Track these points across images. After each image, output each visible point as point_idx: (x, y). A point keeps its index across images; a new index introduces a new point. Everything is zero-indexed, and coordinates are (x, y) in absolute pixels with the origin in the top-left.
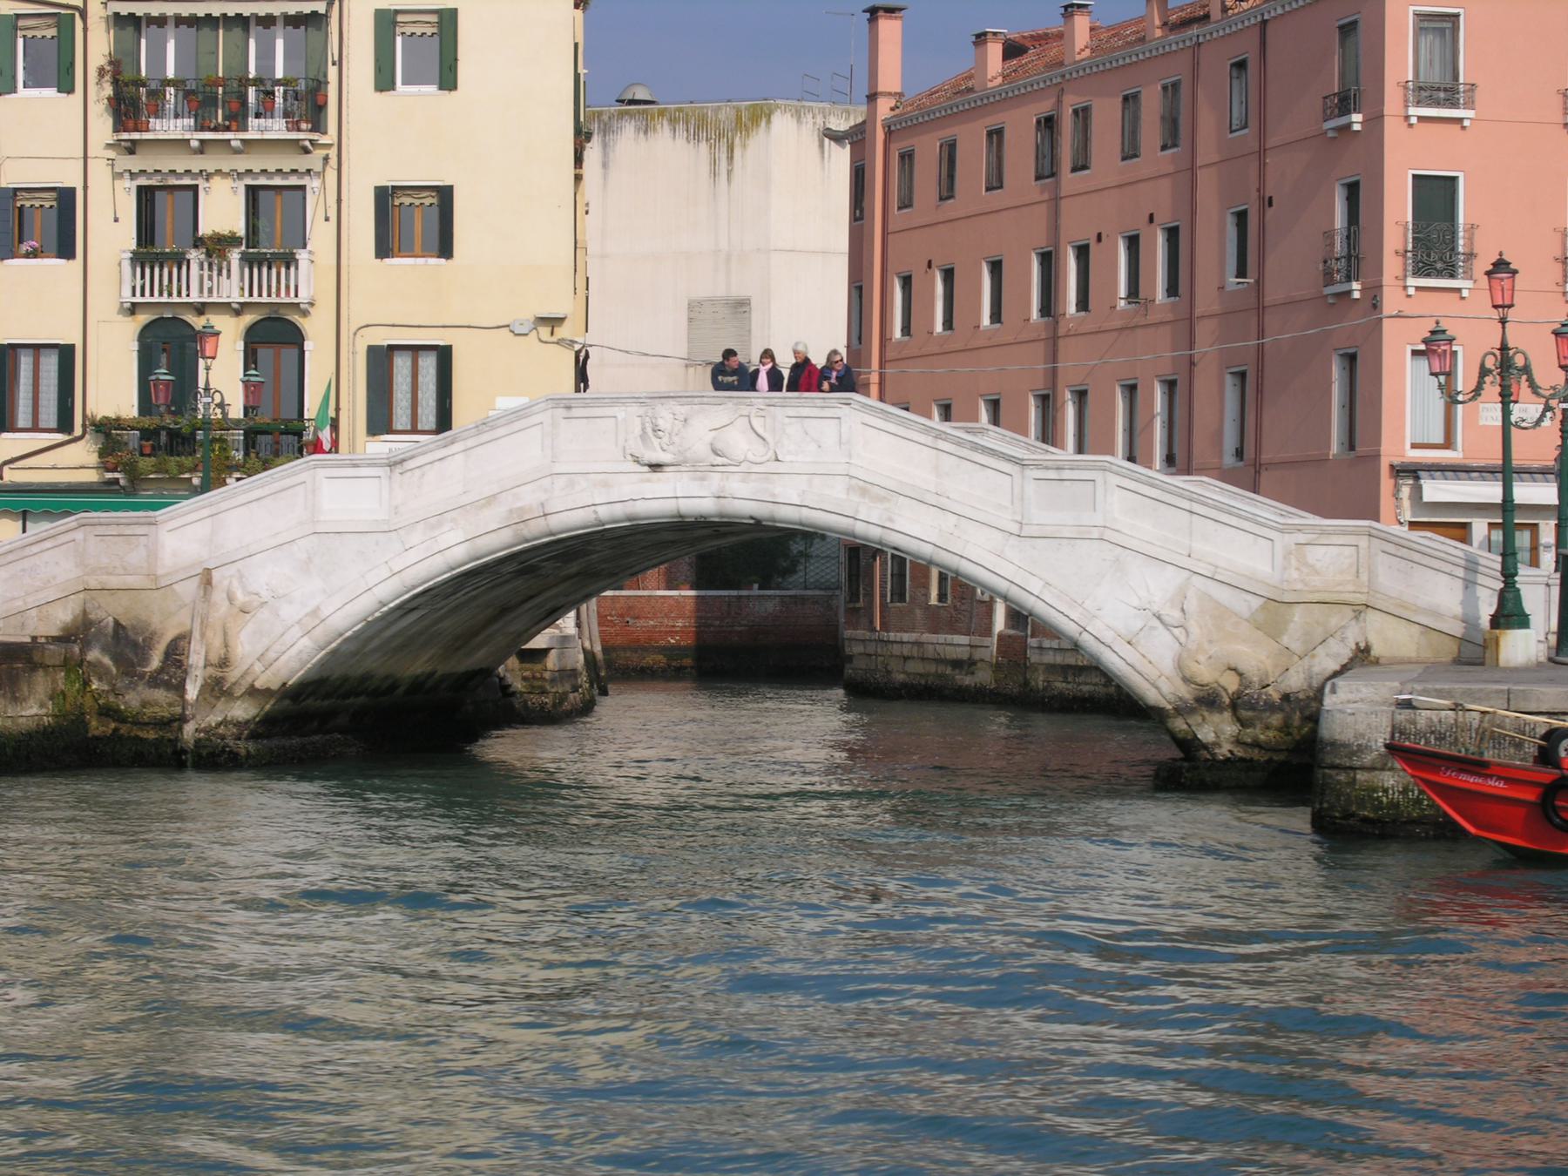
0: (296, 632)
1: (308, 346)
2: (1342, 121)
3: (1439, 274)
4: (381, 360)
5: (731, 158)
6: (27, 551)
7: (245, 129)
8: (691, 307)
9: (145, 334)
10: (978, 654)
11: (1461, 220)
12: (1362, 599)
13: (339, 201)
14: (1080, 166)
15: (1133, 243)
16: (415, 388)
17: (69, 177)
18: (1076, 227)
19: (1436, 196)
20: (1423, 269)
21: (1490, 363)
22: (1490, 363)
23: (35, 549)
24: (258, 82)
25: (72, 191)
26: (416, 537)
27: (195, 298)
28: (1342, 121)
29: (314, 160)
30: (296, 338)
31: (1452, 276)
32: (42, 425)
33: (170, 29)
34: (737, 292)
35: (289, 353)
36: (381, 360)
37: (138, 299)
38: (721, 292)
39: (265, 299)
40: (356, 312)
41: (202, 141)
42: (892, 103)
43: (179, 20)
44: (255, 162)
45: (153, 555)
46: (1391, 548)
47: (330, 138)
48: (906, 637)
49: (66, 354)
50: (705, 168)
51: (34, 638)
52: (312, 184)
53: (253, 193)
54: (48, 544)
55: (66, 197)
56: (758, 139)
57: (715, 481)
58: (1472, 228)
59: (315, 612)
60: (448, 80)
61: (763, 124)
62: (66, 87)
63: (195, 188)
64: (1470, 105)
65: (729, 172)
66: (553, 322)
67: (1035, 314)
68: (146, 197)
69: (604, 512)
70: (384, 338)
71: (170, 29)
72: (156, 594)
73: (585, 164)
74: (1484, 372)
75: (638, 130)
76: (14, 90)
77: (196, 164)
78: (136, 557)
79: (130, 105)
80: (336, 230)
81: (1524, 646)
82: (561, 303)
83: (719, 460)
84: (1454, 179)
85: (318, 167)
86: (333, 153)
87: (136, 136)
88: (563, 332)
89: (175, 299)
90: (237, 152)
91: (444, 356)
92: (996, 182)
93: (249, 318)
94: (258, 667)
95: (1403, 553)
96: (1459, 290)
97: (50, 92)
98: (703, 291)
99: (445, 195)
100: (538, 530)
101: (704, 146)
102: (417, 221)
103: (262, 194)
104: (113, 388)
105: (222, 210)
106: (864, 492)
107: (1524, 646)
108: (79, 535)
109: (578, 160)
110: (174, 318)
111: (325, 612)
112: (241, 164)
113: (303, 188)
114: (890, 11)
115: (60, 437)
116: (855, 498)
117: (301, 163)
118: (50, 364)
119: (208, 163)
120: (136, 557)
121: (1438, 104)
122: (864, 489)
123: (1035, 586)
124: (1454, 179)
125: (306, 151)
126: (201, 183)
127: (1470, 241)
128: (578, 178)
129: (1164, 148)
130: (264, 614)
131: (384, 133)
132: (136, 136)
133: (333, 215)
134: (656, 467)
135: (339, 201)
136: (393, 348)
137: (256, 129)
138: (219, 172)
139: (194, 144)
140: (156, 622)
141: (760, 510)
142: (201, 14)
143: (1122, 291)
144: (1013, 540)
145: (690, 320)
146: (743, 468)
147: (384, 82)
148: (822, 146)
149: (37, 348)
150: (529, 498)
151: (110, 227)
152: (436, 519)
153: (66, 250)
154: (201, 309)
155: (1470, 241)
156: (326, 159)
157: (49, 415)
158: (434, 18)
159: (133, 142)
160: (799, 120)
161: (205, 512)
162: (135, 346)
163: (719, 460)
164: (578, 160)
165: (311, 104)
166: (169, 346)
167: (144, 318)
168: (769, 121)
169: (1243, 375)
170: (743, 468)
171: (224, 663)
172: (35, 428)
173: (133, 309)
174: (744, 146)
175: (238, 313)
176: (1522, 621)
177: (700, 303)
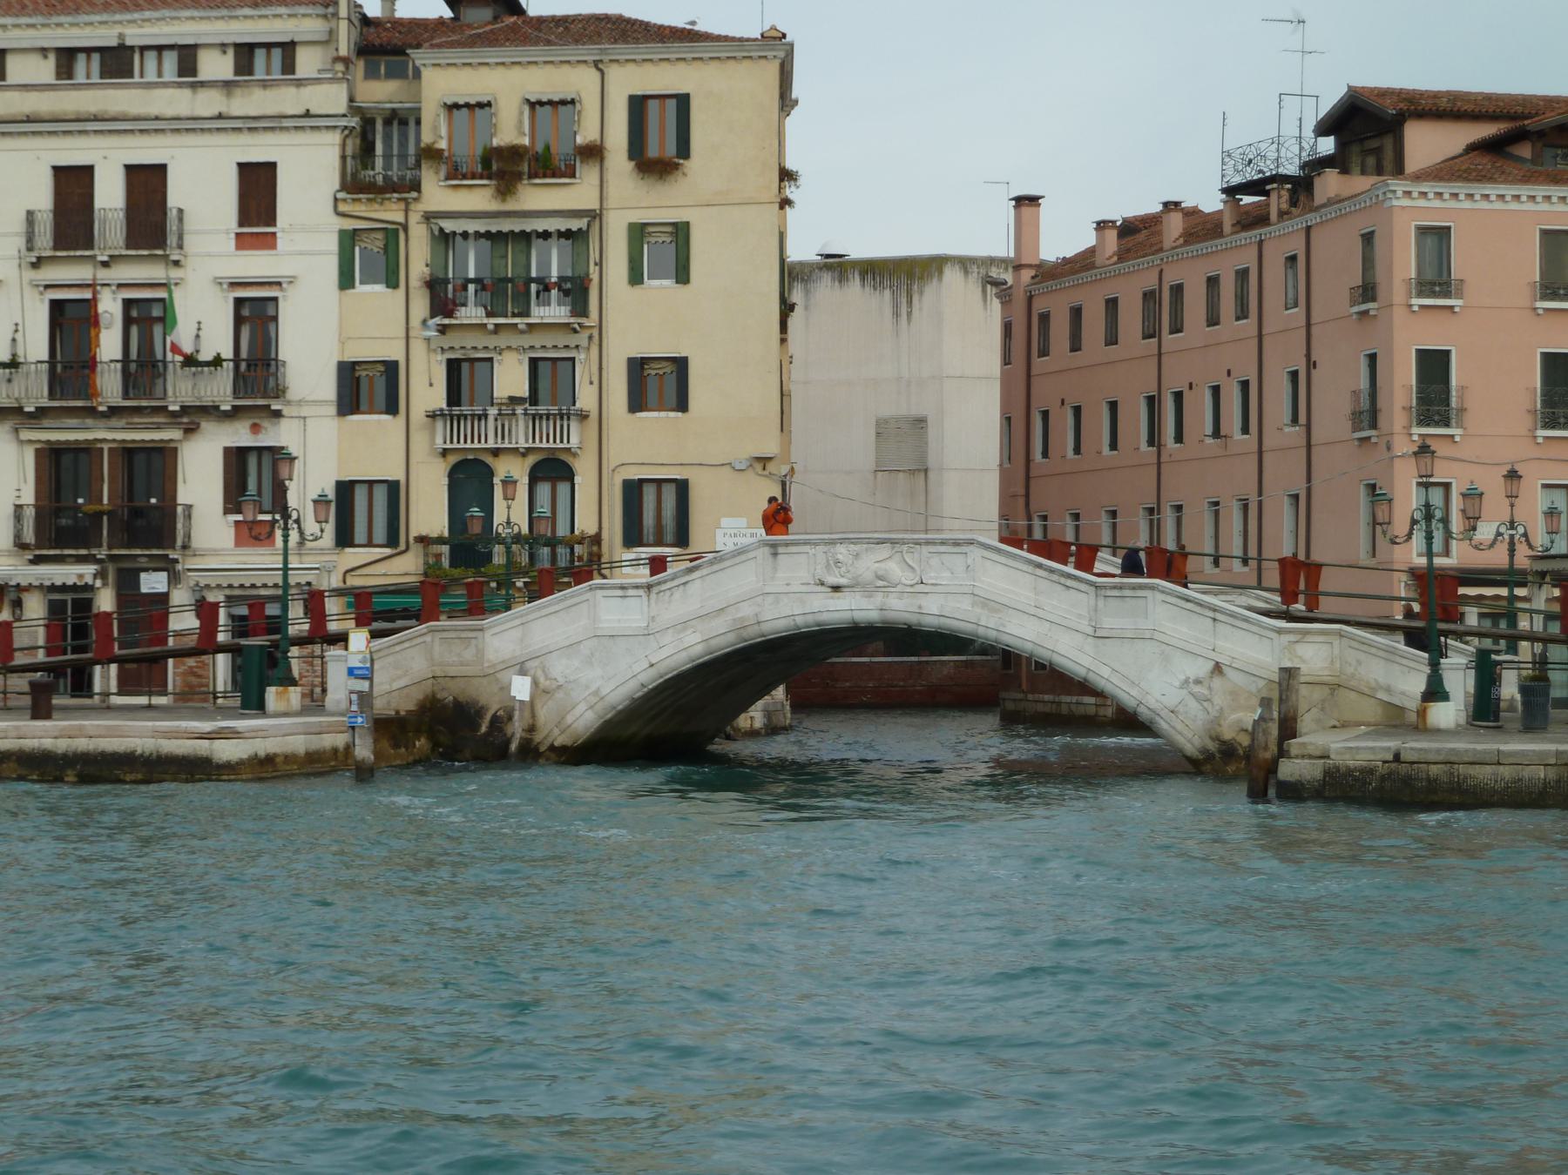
0: (582, 707)
1: (577, 479)
2: (1364, 307)
3: (1437, 424)
4: (633, 491)
5: (910, 303)
6: (392, 650)
7: (527, 315)
8: (878, 423)
9: (452, 474)
10: (1102, 712)
11: (1454, 382)
12: (1335, 680)
13: (600, 369)
14: (1177, 328)
15: (1216, 391)
16: (659, 518)
17: (394, 352)
18: (1172, 383)
19: (1434, 366)
20: (1425, 421)
21: (1418, 516)
22: (1418, 516)
23: (398, 648)
24: (538, 280)
25: (396, 363)
26: (668, 638)
27: (491, 444)
28: (1364, 307)
29: (582, 339)
30: (567, 474)
31: (1447, 425)
32: (375, 541)
33: (471, 241)
34: (916, 411)
35: (563, 488)
36: (633, 491)
37: (448, 446)
38: (903, 411)
39: (545, 445)
40: (613, 456)
41: (496, 325)
42: (1033, 273)
43: (478, 235)
44: (536, 340)
45: (480, 653)
46: (1354, 644)
47: (592, 320)
48: (1047, 697)
49: (393, 488)
50: (888, 311)
51: (397, 712)
52: (580, 357)
53: (534, 363)
54: (406, 645)
55: (391, 368)
56: (931, 290)
57: (879, 599)
58: (1462, 388)
59: (596, 693)
60: (682, 275)
61: (935, 280)
62: (392, 283)
63: (491, 360)
64: (1460, 296)
65: (909, 314)
66: (764, 461)
67: (1144, 446)
68: (453, 367)
69: (800, 621)
70: (635, 474)
71: (471, 241)
72: (485, 681)
73: (790, 330)
74: (1414, 522)
75: (833, 279)
76: (353, 287)
77: (492, 341)
78: (469, 654)
79: (442, 300)
80: (601, 386)
81: (1447, 714)
82: (770, 447)
83: (881, 583)
84: (1448, 352)
85: (584, 343)
86: (595, 333)
87: (446, 321)
88: (771, 467)
89: (476, 445)
90: (522, 332)
91: (682, 487)
92: (1112, 339)
93: (531, 460)
94: (556, 732)
95: (1364, 648)
96: (1452, 436)
97: (380, 288)
98: (888, 411)
99: (681, 364)
100: (753, 634)
101: (887, 293)
102: (660, 383)
103: (541, 364)
104: (429, 512)
105: (511, 378)
106: (984, 606)
107: (1447, 714)
108: (428, 638)
109: (784, 327)
110: (475, 460)
111: (604, 692)
112: (527, 340)
113: (573, 359)
114: (1033, 200)
115: (388, 551)
116: (978, 610)
117: (572, 340)
118: (381, 495)
119: (502, 340)
120: (469, 654)
121: (1434, 295)
122: (986, 603)
123: (1105, 672)
124: (1448, 352)
125: (575, 331)
126: (496, 358)
127: (1461, 398)
128: (783, 341)
129: (1238, 319)
130: (559, 695)
131: (636, 318)
132: (446, 321)
133: (596, 380)
134: (836, 588)
135: (600, 369)
136: (642, 481)
137: (540, 314)
138: (509, 348)
139: (491, 327)
140: (483, 701)
141: (913, 619)
142: (494, 230)
143: (1209, 430)
144: (1090, 640)
145: (878, 434)
146: (899, 588)
147: (636, 278)
148: (984, 291)
149: (371, 483)
150: (747, 611)
151: (426, 388)
152: (684, 625)
153: (392, 408)
154: (496, 452)
155: (1461, 398)
156: (590, 337)
157: (380, 534)
158: (669, 229)
159: (445, 326)
160: (966, 272)
161: (517, 622)
162: (446, 481)
163: (881, 583)
164: (784, 327)
165: (576, 291)
166: (470, 480)
167: (453, 459)
168: (941, 272)
169: (1296, 497)
170: (899, 588)
171: (532, 729)
172: (370, 544)
173: (445, 453)
174: (921, 293)
175: (524, 455)
176: (1444, 697)
177: (886, 421)
